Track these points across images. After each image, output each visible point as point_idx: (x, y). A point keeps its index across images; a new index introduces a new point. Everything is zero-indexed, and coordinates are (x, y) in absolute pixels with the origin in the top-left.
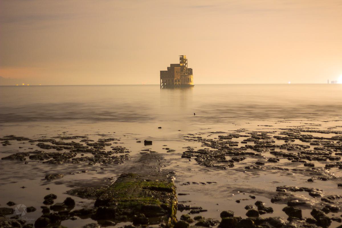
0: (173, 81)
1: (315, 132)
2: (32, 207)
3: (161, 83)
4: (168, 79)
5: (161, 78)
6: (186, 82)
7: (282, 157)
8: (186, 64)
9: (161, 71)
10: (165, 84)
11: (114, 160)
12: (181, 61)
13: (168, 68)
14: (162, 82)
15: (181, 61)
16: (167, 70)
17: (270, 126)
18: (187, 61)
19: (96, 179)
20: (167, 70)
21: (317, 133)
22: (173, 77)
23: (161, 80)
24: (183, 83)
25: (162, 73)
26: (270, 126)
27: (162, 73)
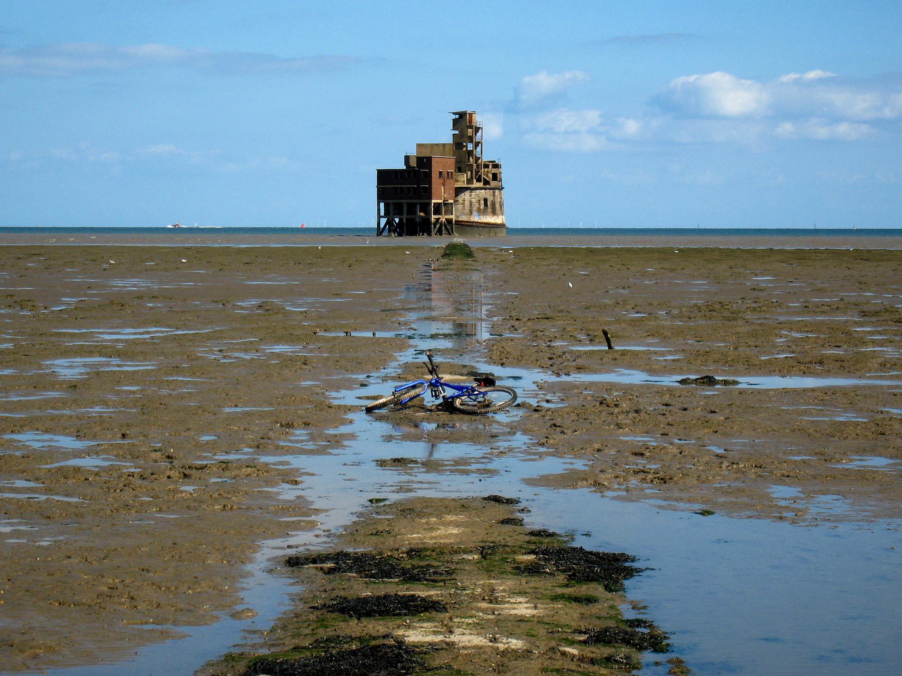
0: (425, 208)
1: (426, 489)
2: (623, 554)
3: (379, 217)
4: (409, 201)
5: (380, 198)
6: (475, 213)
7: (75, 439)
8: (477, 144)
9: (378, 170)
10: (397, 220)
11: (617, 393)
12: (457, 132)
13: (407, 158)
14: (382, 213)
15: (457, 132)
16: (405, 168)
17: (566, 463)
18: (479, 134)
19: (520, 458)
20: (405, 168)
21: (446, 493)
22: (428, 193)
23: (382, 205)
24: (464, 218)
25: (384, 176)
26: (566, 463)
27: (384, 176)
